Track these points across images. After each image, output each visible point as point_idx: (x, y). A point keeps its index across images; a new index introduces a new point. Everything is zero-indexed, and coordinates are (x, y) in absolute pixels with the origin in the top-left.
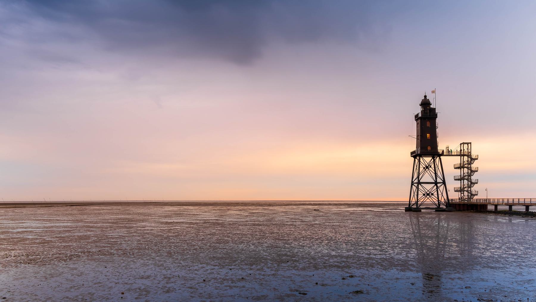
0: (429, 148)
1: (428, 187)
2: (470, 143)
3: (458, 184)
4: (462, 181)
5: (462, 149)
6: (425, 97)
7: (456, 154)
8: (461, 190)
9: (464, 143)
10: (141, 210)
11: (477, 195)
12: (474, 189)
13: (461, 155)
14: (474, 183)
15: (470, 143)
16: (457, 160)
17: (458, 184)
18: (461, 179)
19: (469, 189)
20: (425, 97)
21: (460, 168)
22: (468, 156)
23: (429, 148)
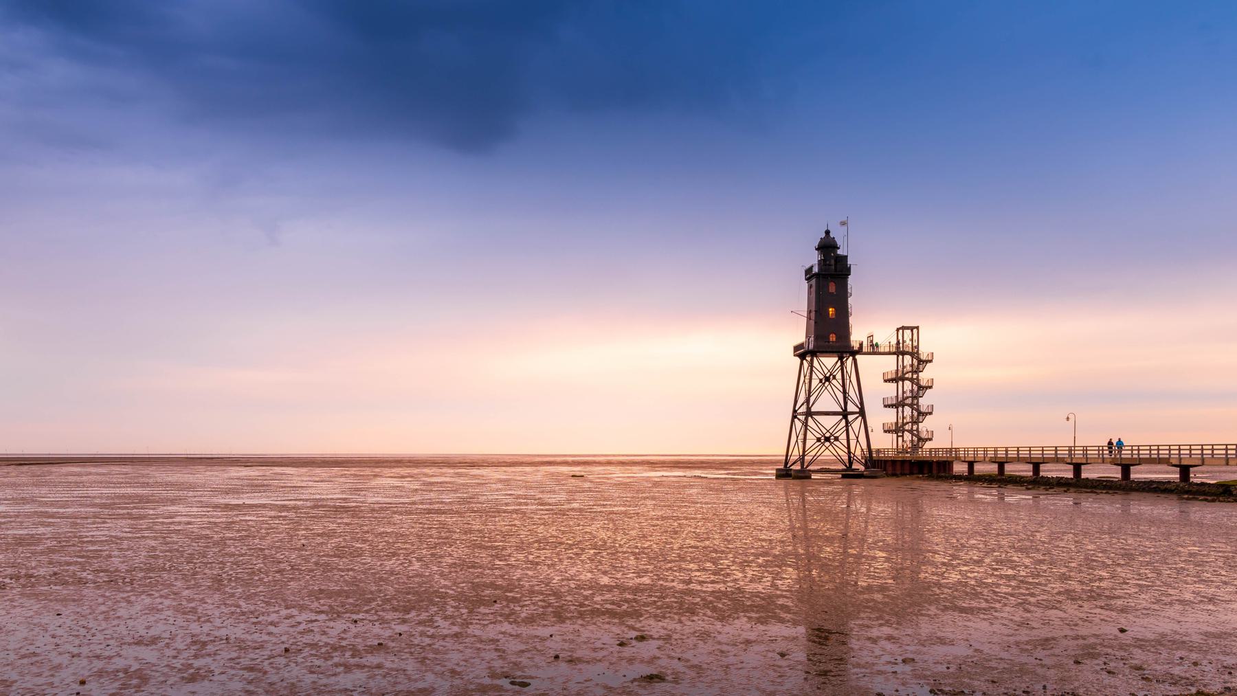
1: (828, 422)
2: (917, 328)
6: (827, 232)
7: (887, 350)
12: (926, 425)
13: (899, 352)
15: (917, 328)
16: (889, 364)
22: (912, 354)
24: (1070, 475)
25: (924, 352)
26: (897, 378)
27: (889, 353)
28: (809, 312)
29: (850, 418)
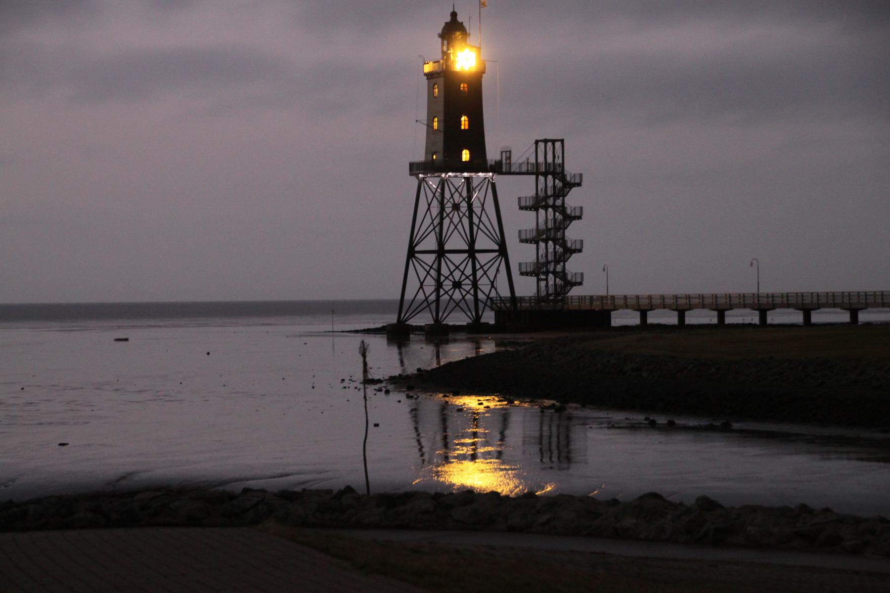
0: (466, 155)
1: (457, 258)
2: (562, 141)
3: (529, 221)
4: (542, 245)
5: (546, 433)
6: (454, 15)
7: (524, 169)
8: (538, 270)
9: (546, 141)
10: (93, 343)
11: (580, 284)
12: (573, 265)
13: (535, 171)
14: (573, 218)
15: (562, 141)
16: (527, 187)
17: (529, 221)
18: (537, 204)
19: (559, 235)
20: (454, 15)
21: (535, 207)
22: (555, 175)
23: (466, 155)
24: (715, 321)
25: (570, 169)
26: (537, 204)
27: (527, 173)
28: (199, 326)
29: (482, 258)
